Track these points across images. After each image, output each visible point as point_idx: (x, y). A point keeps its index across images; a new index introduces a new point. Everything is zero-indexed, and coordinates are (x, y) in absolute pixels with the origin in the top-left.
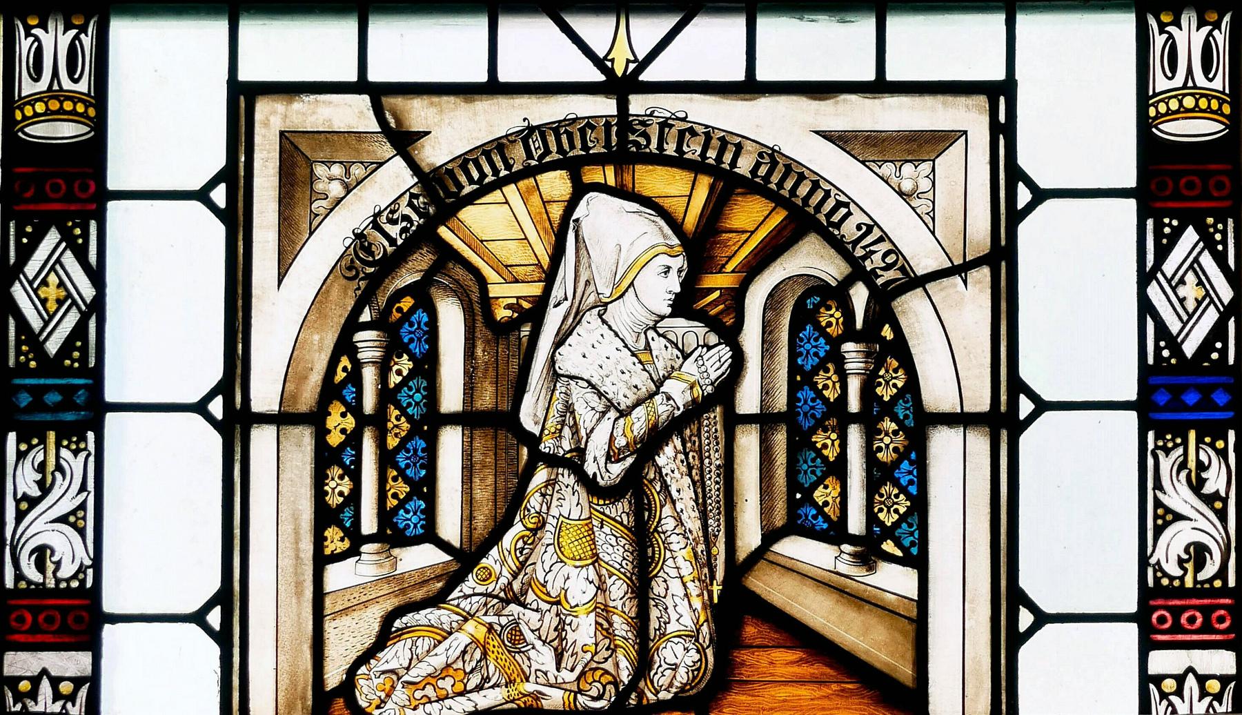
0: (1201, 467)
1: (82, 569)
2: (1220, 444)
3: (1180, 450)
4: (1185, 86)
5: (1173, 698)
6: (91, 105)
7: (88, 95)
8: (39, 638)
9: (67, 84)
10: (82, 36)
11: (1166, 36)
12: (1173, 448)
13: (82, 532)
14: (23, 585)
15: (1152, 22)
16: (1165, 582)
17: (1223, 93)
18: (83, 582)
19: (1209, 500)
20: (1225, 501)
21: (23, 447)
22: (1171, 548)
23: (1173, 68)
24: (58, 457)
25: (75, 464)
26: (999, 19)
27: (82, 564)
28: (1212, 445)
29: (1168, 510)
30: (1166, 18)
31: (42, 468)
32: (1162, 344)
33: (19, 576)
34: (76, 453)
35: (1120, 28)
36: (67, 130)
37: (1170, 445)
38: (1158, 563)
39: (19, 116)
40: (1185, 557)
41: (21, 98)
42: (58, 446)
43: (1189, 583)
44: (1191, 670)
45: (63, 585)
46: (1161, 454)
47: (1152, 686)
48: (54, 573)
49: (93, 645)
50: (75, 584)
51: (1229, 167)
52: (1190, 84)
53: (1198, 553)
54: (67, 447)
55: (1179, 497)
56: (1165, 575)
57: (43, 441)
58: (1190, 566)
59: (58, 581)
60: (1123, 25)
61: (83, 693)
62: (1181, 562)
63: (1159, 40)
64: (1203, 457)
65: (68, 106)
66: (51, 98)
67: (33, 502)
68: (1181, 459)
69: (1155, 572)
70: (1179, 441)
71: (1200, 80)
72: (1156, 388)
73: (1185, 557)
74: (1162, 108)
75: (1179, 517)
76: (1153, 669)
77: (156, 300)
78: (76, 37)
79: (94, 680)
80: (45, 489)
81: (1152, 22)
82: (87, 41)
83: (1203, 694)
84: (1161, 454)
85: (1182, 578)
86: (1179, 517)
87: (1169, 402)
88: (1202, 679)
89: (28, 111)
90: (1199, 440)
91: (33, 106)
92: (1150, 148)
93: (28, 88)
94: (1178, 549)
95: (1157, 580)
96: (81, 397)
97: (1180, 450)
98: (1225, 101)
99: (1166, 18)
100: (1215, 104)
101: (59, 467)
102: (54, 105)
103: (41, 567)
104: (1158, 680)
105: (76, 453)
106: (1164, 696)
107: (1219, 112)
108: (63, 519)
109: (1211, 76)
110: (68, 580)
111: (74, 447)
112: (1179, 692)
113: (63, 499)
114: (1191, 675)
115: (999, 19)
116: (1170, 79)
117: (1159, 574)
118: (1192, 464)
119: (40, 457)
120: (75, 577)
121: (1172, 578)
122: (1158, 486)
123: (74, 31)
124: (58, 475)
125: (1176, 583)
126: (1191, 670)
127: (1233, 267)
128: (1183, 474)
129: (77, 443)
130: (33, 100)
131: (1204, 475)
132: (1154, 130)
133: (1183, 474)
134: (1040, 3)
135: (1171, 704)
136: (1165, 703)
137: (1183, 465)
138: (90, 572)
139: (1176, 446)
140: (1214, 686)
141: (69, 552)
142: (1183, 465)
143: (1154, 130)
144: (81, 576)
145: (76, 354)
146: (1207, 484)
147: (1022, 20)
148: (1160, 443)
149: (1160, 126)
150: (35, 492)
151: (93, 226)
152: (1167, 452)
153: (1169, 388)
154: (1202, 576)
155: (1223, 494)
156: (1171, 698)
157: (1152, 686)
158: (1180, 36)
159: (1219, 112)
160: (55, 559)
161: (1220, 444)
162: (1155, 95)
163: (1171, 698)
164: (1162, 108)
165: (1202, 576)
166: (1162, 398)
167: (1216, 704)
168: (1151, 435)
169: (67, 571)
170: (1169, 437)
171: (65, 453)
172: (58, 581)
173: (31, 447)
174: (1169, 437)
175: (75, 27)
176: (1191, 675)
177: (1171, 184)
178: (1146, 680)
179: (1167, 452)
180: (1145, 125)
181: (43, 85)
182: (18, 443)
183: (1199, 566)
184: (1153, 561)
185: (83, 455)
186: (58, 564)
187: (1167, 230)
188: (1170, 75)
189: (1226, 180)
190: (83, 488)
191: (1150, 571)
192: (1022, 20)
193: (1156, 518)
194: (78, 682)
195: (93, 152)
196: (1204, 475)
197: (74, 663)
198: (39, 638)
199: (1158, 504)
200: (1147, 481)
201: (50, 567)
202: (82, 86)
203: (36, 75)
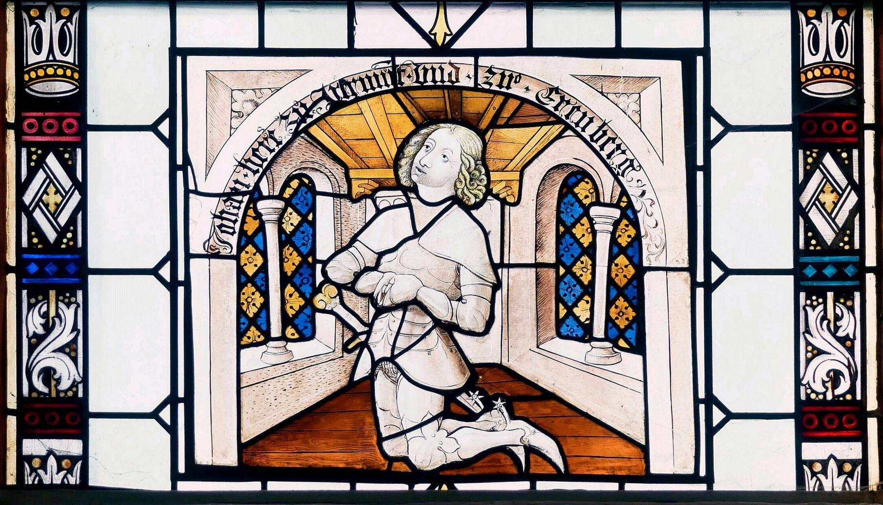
0: (837, 318)
1: (74, 384)
2: (849, 303)
3: (821, 307)
4: (47, 60)
5: (40, 472)
6: (76, 71)
7: (74, 64)
8: (844, 433)
9: (59, 56)
10: (845, 24)
11: (34, 26)
12: (816, 306)
13: (75, 360)
14: (34, 395)
15: (802, 17)
16: (813, 396)
17: (851, 65)
18: (76, 393)
19: (842, 340)
20: (853, 341)
21: (33, 301)
22: (816, 375)
23: (817, 48)
24: (57, 308)
25: (69, 314)
26: (522, 13)
27: (74, 381)
28: (844, 304)
29: (814, 348)
30: (33, 13)
31: (45, 315)
32: (33, 233)
33: (32, 388)
34: (68, 305)
35: (780, 20)
36: (62, 87)
37: (815, 303)
38: (808, 383)
39: (803, 79)
40: (826, 379)
41: (28, 66)
42: (57, 300)
43: (829, 397)
44: (832, 456)
45: (62, 395)
46: (809, 309)
47: (805, 467)
48: (56, 386)
49: (82, 434)
50: (70, 394)
51: (855, 115)
52: (51, 58)
53: (835, 377)
54: (63, 301)
55: (821, 338)
56: (813, 391)
57: (47, 298)
58: (829, 385)
59: (58, 392)
60: (782, 18)
61: (859, 469)
62: (824, 382)
63: (30, 30)
64: (838, 311)
65: (60, 72)
66: (825, 67)
67: (40, 338)
68: (822, 313)
69: (806, 389)
70: (820, 300)
71: (59, 56)
72: (806, 265)
73: (826, 379)
74: (33, 75)
75: (821, 352)
76: (805, 456)
77: (124, 201)
78: (65, 24)
79: (84, 457)
80: (48, 328)
81: (802, 17)
82: (849, 29)
83: (841, 472)
84: (809, 309)
85: (824, 394)
86: (821, 352)
87: (836, 274)
88: (59, 459)
89: (810, 75)
90: (836, 300)
91: (813, 72)
92: (800, 100)
93: (809, 59)
94: (822, 374)
95: (808, 395)
96: (72, 268)
97: (821, 307)
98: (76, 71)
99: (812, 13)
100: (69, 73)
101: (58, 315)
102: (827, 71)
103: (47, 383)
104: (810, 464)
105: (68, 305)
106: (814, 474)
107: (72, 77)
108: (61, 350)
109: (842, 54)
110: (66, 391)
111: (67, 300)
112: (824, 472)
113: (63, 336)
114: (52, 457)
115: (522, 13)
116: (38, 54)
117: (809, 391)
118: (831, 315)
119: (44, 309)
120: (70, 389)
121: (817, 394)
122: (808, 331)
123: (840, 21)
124: (57, 320)
125: (821, 397)
126: (832, 456)
127: (857, 181)
128: (825, 322)
129: (69, 298)
130: (813, 67)
131: (838, 324)
132: (803, 91)
133: (825, 322)
134: (675, 3)
135: (818, 479)
136: (815, 479)
137: (824, 318)
138: (81, 386)
139: (819, 304)
140: (848, 467)
141: (67, 372)
142: (824, 318)
143: (803, 91)
144: (74, 389)
145: (846, 239)
146: (841, 330)
147: (537, 13)
148: (809, 302)
149: (850, 87)
150: (40, 331)
151: (79, 151)
152: (814, 308)
153: (815, 265)
154: (838, 392)
155: (851, 337)
156: (819, 475)
157: (805, 467)
158: (45, 26)
159: (848, 78)
160: (56, 377)
161: (849, 303)
162: (28, 66)
163: (819, 475)
164: (810, 75)
165: (838, 392)
166: (810, 272)
167: (849, 480)
168: (802, 295)
169: (65, 385)
170: (68, 295)
171: (61, 305)
172: (58, 392)
173: (38, 302)
174: (814, 298)
175: (839, 18)
176: (52, 457)
177: (816, 126)
178: (800, 463)
179: (814, 308)
180: (797, 85)
181: (43, 56)
182: (29, 297)
183: (836, 385)
184: (804, 382)
185: (73, 307)
186: (58, 381)
187: (34, 157)
188: (814, 52)
189: (75, 123)
190: (75, 328)
191: (802, 389)
192: (626, 14)
193: (804, 352)
194: (855, 463)
195: (78, 101)
196: (838, 324)
197: (74, 447)
198: (844, 433)
199: (808, 344)
200: (800, 330)
201: (53, 383)
202: (847, 59)
203: (38, 50)
